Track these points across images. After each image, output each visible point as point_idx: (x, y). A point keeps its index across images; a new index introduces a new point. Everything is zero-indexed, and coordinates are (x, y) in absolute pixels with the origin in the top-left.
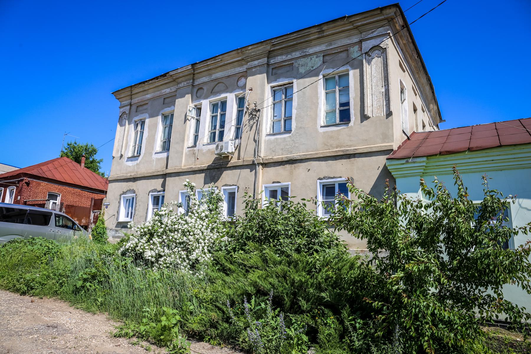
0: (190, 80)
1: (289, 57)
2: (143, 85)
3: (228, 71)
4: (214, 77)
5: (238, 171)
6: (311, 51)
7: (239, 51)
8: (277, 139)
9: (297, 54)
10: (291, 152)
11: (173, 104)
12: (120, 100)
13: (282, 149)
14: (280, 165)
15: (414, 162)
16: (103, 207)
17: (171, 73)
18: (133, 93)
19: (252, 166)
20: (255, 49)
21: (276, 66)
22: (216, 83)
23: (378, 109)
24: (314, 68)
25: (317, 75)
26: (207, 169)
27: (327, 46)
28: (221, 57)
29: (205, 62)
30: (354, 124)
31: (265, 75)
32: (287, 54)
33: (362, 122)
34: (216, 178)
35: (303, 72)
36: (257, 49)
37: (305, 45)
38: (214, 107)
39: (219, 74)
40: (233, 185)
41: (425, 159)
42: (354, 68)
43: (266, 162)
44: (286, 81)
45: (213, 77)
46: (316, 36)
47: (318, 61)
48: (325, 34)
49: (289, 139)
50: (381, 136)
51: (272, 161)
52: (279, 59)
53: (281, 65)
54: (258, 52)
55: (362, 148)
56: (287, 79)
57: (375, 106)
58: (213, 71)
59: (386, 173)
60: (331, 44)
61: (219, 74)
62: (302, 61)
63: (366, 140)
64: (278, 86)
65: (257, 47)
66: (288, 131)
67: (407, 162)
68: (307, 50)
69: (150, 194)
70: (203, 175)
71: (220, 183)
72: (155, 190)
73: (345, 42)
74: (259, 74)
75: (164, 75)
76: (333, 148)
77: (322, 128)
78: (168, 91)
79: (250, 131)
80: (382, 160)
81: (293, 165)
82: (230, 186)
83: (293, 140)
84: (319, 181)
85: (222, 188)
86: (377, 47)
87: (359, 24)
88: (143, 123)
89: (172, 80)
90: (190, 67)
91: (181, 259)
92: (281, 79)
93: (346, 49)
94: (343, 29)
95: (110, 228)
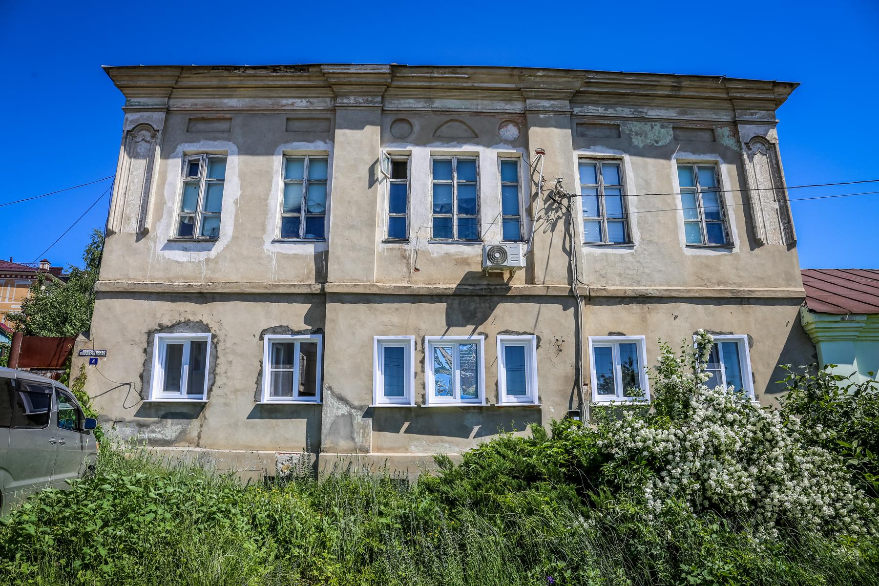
0: (374, 95)
1: (611, 112)
2: (226, 73)
3: (475, 102)
4: (438, 104)
5: (534, 307)
6: (653, 113)
7: (516, 72)
8: (606, 254)
9: (626, 112)
10: (639, 283)
11: (330, 137)
12: (127, 91)
13: (620, 275)
14: (620, 303)
15: (851, 321)
16: (77, 361)
17: (326, 69)
18: (181, 84)
19: (569, 299)
20: (549, 79)
21: (585, 120)
22: (446, 118)
23: (774, 234)
24: (660, 144)
25: (668, 157)
26: (454, 295)
27: (678, 113)
28: (470, 71)
29: (426, 70)
30: (741, 249)
31: (379, 128)
32: (607, 106)
33: (752, 249)
34: (479, 315)
35: (641, 145)
36: (554, 80)
37: (642, 100)
38: (440, 166)
39: (452, 103)
40: (525, 333)
41: (865, 318)
42: (728, 161)
43: (592, 294)
44: (609, 154)
45: (435, 105)
46: (666, 93)
47: (666, 136)
48: (682, 93)
49: (631, 259)
50: (784, 276)
51: (605, 294)
52: (591, 110)
53: (597, 121)
54: (553, 86)
55: (760, 290)
56: (611, 150)
57: (768, 227)
58: (440, 93)
59: (799, 332)
60: (686, 114)
61: (452, 103)
62: (636, 126)
63: (762, 279)
64: (591, 158)
65: (555, 77)
66: (627, 241)
67: (843, 319)
68: (645, 110)
69: (266, 337)
70: (443, 306)
71: (488, 326)
72: (285, 329)
73: (709, 116)
74: (556, 127)
75: (303, 68)
76: (714, 284)
77: (689, 249)
78: (301, 104)
79: (552, 230)
80: (791, 312)
81: (646, 306)
82: (518, 334)
83: (639, 262)
84: (413, 338)
85: (499, 337)
86: (761, 139)
87: (738, 95)
88: (217, 163)
89: (321, 84)
90: (386, 70)
91: (490, 482)
92: (598, 148)
93: (710, 129)
94: (711, 95)
95: (115, 414)
